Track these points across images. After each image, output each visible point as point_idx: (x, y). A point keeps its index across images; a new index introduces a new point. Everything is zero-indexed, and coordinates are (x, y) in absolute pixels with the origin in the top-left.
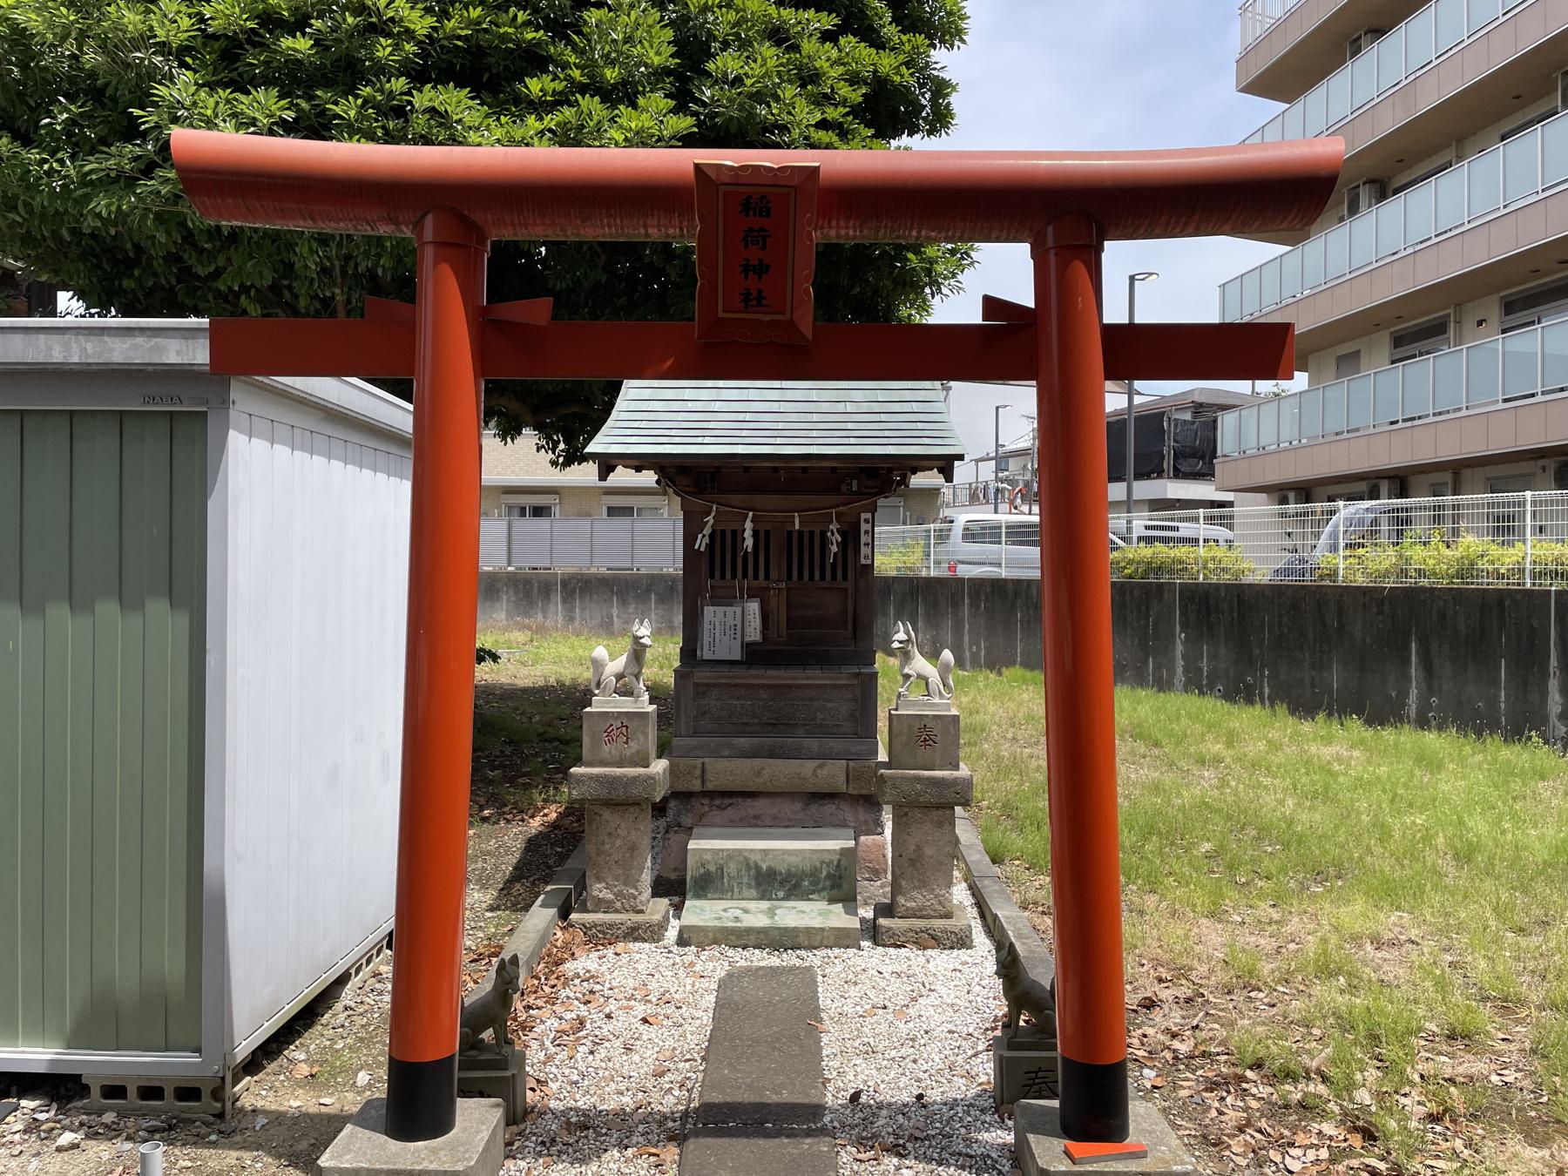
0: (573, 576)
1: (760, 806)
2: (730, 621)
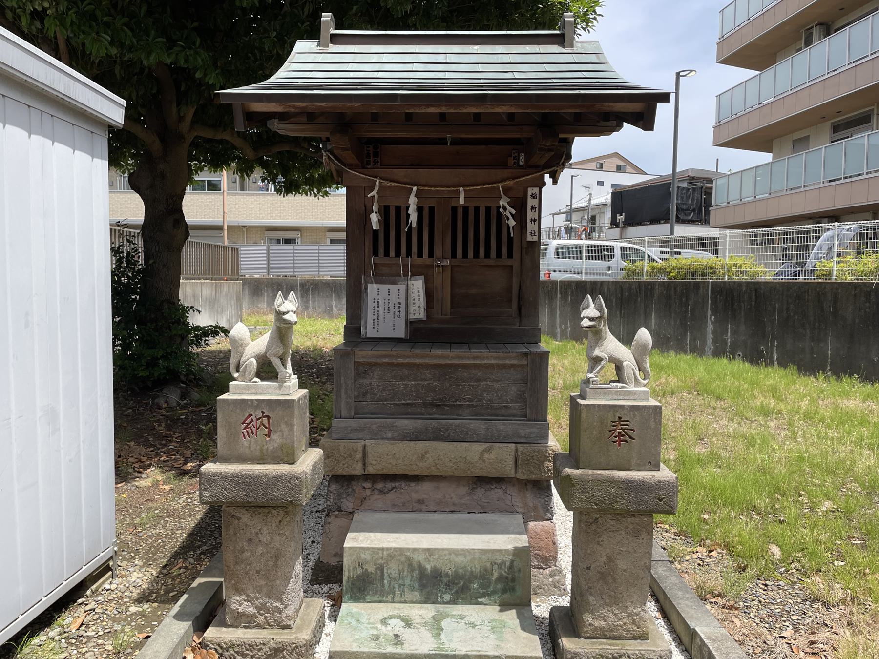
0: (307, 281)
1: (425, 489)
2: (394, 299)
